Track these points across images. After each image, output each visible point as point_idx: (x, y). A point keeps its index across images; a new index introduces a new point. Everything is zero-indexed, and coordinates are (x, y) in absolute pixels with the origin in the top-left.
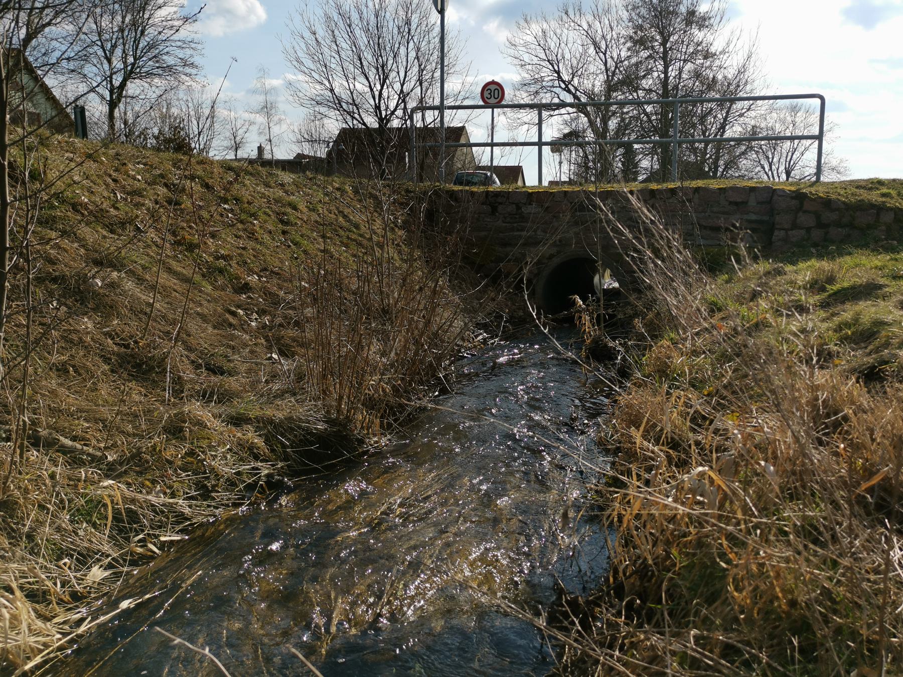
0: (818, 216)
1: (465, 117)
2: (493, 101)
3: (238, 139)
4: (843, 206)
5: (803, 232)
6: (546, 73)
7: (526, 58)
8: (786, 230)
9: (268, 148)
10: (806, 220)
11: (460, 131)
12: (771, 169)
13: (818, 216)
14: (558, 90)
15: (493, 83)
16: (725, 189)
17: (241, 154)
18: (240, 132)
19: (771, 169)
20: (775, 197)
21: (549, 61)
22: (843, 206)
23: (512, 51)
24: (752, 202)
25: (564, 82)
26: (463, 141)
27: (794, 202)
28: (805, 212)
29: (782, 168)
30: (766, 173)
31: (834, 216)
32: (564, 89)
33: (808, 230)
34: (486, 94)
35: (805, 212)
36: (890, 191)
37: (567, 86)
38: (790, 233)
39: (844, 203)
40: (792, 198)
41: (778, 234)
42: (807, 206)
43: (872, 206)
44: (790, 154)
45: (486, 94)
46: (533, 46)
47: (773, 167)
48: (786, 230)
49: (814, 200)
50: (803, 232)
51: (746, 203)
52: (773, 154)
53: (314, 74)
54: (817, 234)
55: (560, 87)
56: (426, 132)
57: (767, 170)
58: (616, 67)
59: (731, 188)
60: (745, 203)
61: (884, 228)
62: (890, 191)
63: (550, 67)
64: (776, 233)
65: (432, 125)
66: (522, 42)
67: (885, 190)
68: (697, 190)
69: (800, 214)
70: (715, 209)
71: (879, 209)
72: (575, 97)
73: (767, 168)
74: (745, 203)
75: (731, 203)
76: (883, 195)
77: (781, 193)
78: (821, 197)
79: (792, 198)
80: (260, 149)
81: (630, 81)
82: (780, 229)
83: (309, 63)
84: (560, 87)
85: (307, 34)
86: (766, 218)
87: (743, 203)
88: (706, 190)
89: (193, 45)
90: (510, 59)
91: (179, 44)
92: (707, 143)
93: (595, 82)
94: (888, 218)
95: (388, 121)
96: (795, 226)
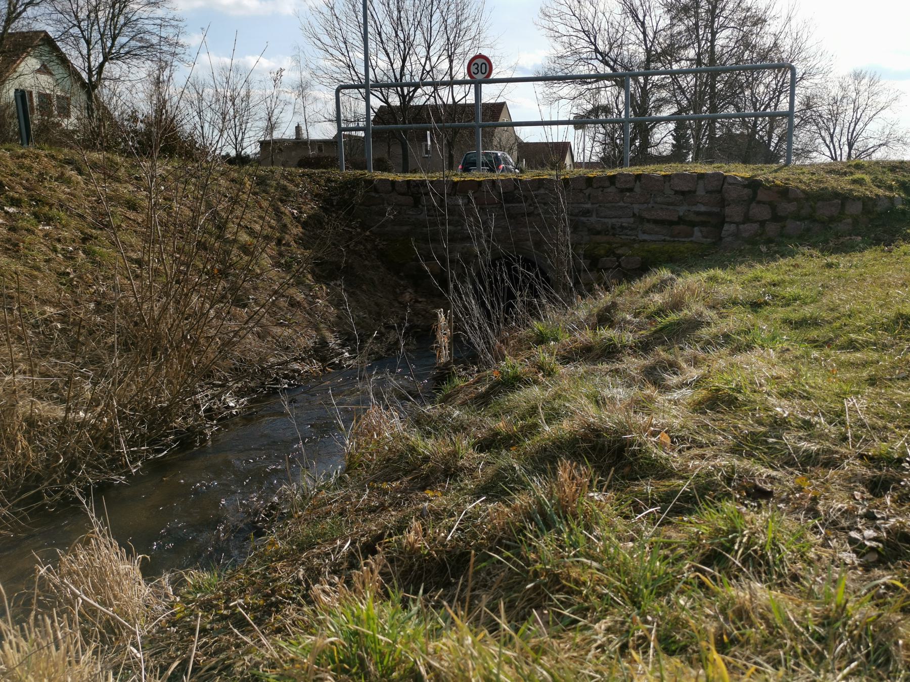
0: (773, 207)
1: (497, 93)
2: (480, 77)
3: (273, 119)
4: (802, 195)
5: (756, 226)
6: (582, 44)
7: (562, 29)
8: (737, 224)
9: (304, 127)
10: (760, 212)
11: (499, 108)
12: (832, 141)
13: (773, 207)
14: (596, 63)
15: (480, 56)
16: (669, 176)
17: (277, 135)
18: (276, 112)
19: (832, 141)
20: (726, 186)
21: (584, 32)
22: (802, 195)
23: (545, 23)
24: (701, 192)
25: (601, 54)
26: (503, 119)
27: (746, 191)
28: (759, 202)
29: (844, 139)
30: (827, 145)
31: (791, 207)
32: (601, 61)
33: (762, 223)
34: (473, 69)
35: (759, 202)
36: (864, 176)
37: (603, 58)
38: (741, 227)
39: (804, 191)
40: (745, 186)
41: (728, 228)
42: (761, 196)
43: (836, 194)
44: (853, 125)
45: (473, 69)
46: (568, 17)
47: (835, 139)
48: (737, 224)
49: (769, 189)
50: (756, 226)
51: (695, 192)
52: (835, 125)
53: (330, 50)
54: (772, 229)
55: (597, 58)
56: (456, 110)
57: (828, 142)
58: (654, 38)
59: (677, 175)
60: (692, 192)
61: (849, 220)
62: (864, 176)
63: (587, 39)
64: (726, 227)
65: (463, 102)
66: (556, 12)
67: (858, 175)
68: (638, 177)
69: (754, 204)
70: (659, 200)
71: (844, 198)
72: (612, 68)
73: (828, 140)
74: (692, 192)
75: (676, 192)
76: (854, 182)
77: (731, 181)
78: (777, 186)
79: (745, 186)
80: (298, 129)
81: (671, 51)
82: (731, 223)
83: (326, 39)
84: (597, 58)
85: (326, 10)
86: (716, 210)
87: (689, 192)
88: (648, 177)
89: (174, 23)
90: (544, 31)
91: (159, 22)
92: (757, 117)
93: (635, 51)
94: (855, 209)
95: (411, 98)
96: (747, 219)
